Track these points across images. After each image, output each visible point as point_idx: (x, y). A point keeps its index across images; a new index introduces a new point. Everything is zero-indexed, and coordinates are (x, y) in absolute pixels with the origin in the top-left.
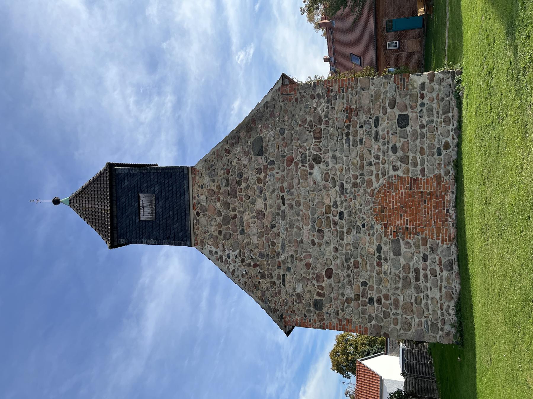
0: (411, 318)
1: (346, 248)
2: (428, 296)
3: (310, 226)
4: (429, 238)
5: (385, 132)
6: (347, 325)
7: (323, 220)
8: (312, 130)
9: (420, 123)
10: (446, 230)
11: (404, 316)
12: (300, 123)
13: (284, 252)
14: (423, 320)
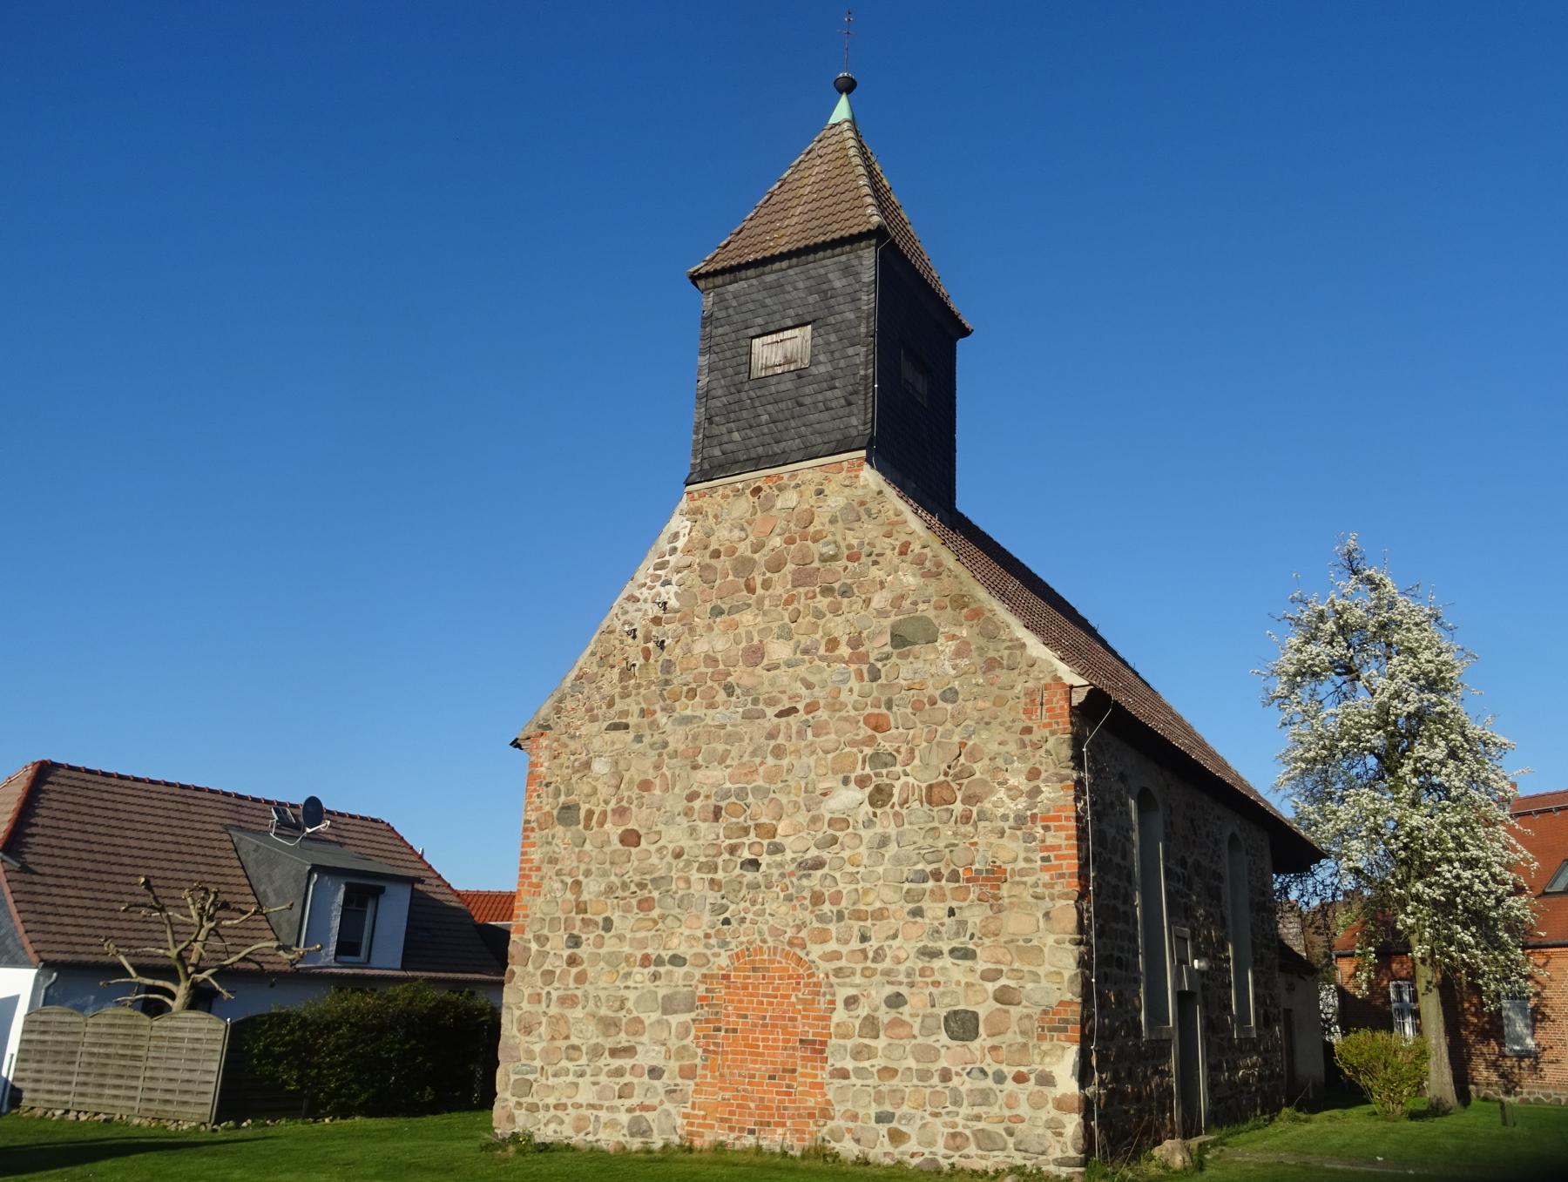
5: (937, 977)
9: (954, 1070)
10: (712, 1127)
14: (538, 1063)
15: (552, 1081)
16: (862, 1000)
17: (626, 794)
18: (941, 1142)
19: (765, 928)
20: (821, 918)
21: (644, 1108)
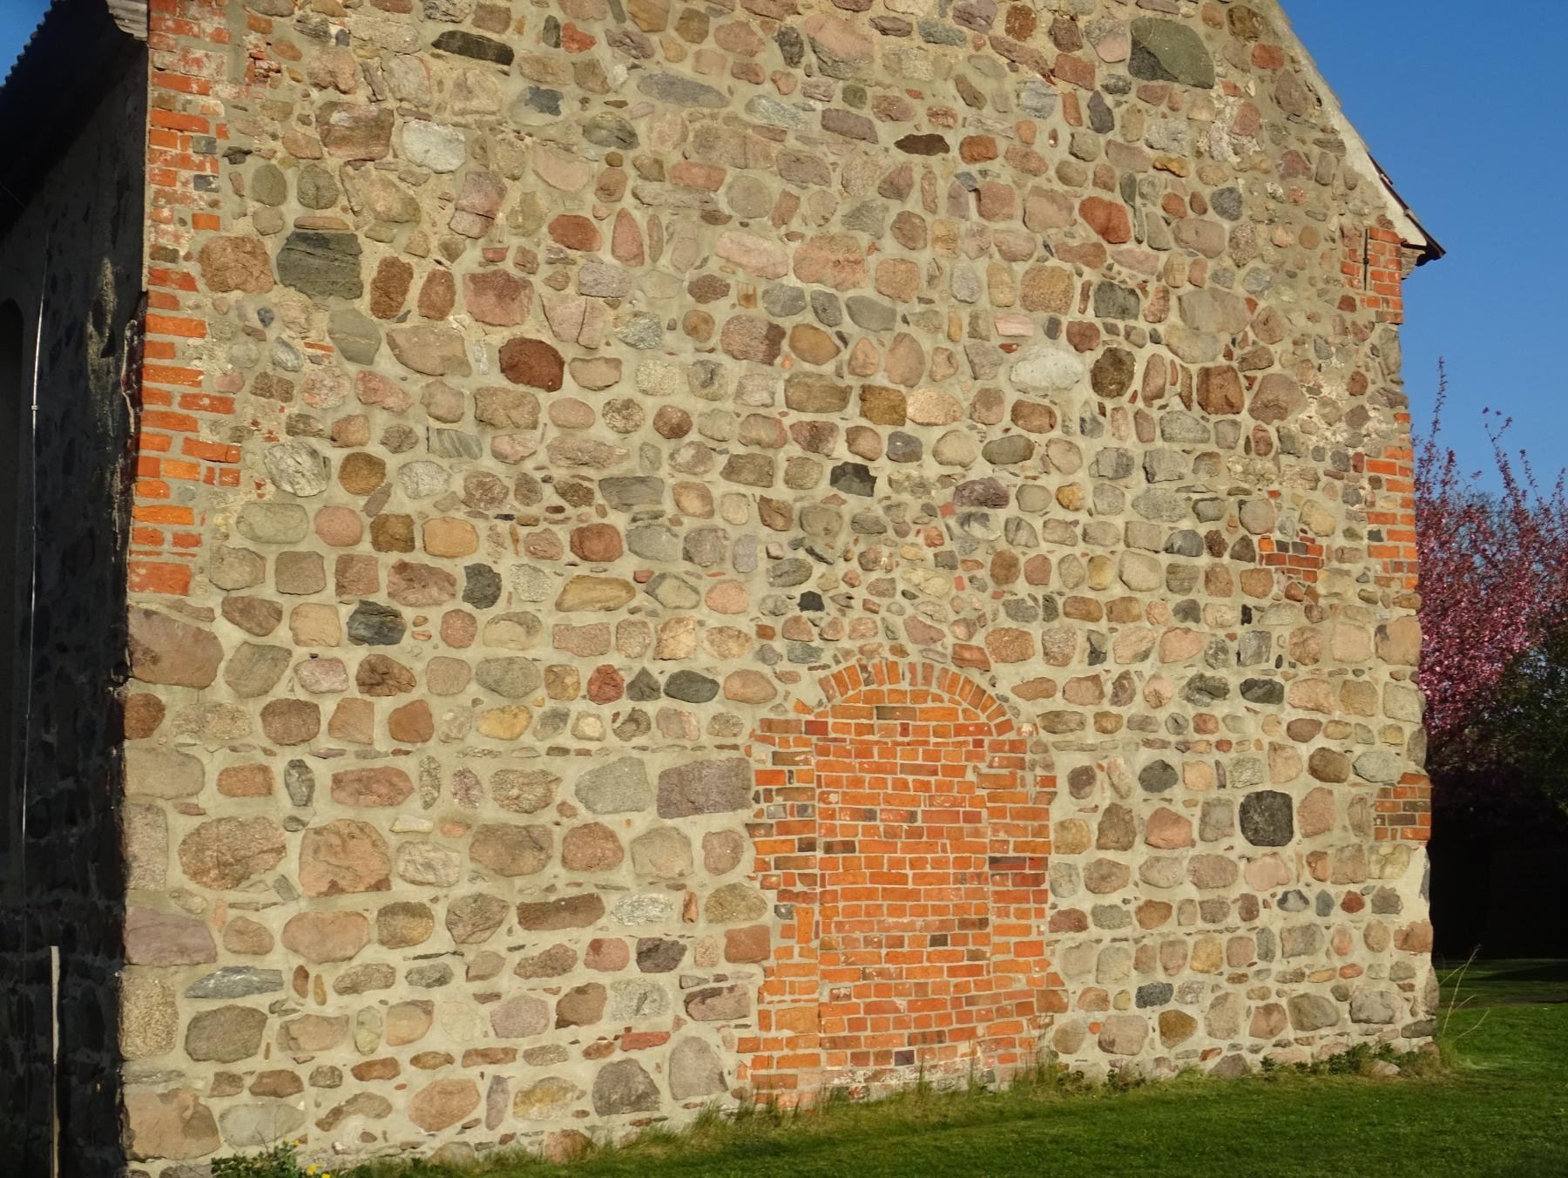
0: (283, 885)
1: (686, 486)
2: (442, 981)
3: (792, 281)
4: (767, 972)
5: (1223, 733)
6: (191, 447)
7: (828, 368)
8: (1235, 364)
9: (1260, 897)
10: (813, 1060)
11: (294, 841)
12: (1262, 304)
13: (647, 84)
14: (280, 960)
15: (335, 1005)
16: (1101, 776)
17: (514, 242)
18: (1245, 1026)
19: (898, 622)
20: (1016, 610)
21: (633, 1040)
